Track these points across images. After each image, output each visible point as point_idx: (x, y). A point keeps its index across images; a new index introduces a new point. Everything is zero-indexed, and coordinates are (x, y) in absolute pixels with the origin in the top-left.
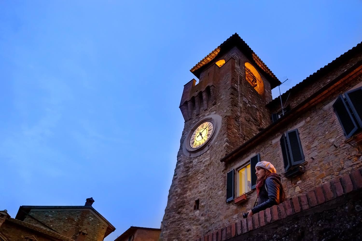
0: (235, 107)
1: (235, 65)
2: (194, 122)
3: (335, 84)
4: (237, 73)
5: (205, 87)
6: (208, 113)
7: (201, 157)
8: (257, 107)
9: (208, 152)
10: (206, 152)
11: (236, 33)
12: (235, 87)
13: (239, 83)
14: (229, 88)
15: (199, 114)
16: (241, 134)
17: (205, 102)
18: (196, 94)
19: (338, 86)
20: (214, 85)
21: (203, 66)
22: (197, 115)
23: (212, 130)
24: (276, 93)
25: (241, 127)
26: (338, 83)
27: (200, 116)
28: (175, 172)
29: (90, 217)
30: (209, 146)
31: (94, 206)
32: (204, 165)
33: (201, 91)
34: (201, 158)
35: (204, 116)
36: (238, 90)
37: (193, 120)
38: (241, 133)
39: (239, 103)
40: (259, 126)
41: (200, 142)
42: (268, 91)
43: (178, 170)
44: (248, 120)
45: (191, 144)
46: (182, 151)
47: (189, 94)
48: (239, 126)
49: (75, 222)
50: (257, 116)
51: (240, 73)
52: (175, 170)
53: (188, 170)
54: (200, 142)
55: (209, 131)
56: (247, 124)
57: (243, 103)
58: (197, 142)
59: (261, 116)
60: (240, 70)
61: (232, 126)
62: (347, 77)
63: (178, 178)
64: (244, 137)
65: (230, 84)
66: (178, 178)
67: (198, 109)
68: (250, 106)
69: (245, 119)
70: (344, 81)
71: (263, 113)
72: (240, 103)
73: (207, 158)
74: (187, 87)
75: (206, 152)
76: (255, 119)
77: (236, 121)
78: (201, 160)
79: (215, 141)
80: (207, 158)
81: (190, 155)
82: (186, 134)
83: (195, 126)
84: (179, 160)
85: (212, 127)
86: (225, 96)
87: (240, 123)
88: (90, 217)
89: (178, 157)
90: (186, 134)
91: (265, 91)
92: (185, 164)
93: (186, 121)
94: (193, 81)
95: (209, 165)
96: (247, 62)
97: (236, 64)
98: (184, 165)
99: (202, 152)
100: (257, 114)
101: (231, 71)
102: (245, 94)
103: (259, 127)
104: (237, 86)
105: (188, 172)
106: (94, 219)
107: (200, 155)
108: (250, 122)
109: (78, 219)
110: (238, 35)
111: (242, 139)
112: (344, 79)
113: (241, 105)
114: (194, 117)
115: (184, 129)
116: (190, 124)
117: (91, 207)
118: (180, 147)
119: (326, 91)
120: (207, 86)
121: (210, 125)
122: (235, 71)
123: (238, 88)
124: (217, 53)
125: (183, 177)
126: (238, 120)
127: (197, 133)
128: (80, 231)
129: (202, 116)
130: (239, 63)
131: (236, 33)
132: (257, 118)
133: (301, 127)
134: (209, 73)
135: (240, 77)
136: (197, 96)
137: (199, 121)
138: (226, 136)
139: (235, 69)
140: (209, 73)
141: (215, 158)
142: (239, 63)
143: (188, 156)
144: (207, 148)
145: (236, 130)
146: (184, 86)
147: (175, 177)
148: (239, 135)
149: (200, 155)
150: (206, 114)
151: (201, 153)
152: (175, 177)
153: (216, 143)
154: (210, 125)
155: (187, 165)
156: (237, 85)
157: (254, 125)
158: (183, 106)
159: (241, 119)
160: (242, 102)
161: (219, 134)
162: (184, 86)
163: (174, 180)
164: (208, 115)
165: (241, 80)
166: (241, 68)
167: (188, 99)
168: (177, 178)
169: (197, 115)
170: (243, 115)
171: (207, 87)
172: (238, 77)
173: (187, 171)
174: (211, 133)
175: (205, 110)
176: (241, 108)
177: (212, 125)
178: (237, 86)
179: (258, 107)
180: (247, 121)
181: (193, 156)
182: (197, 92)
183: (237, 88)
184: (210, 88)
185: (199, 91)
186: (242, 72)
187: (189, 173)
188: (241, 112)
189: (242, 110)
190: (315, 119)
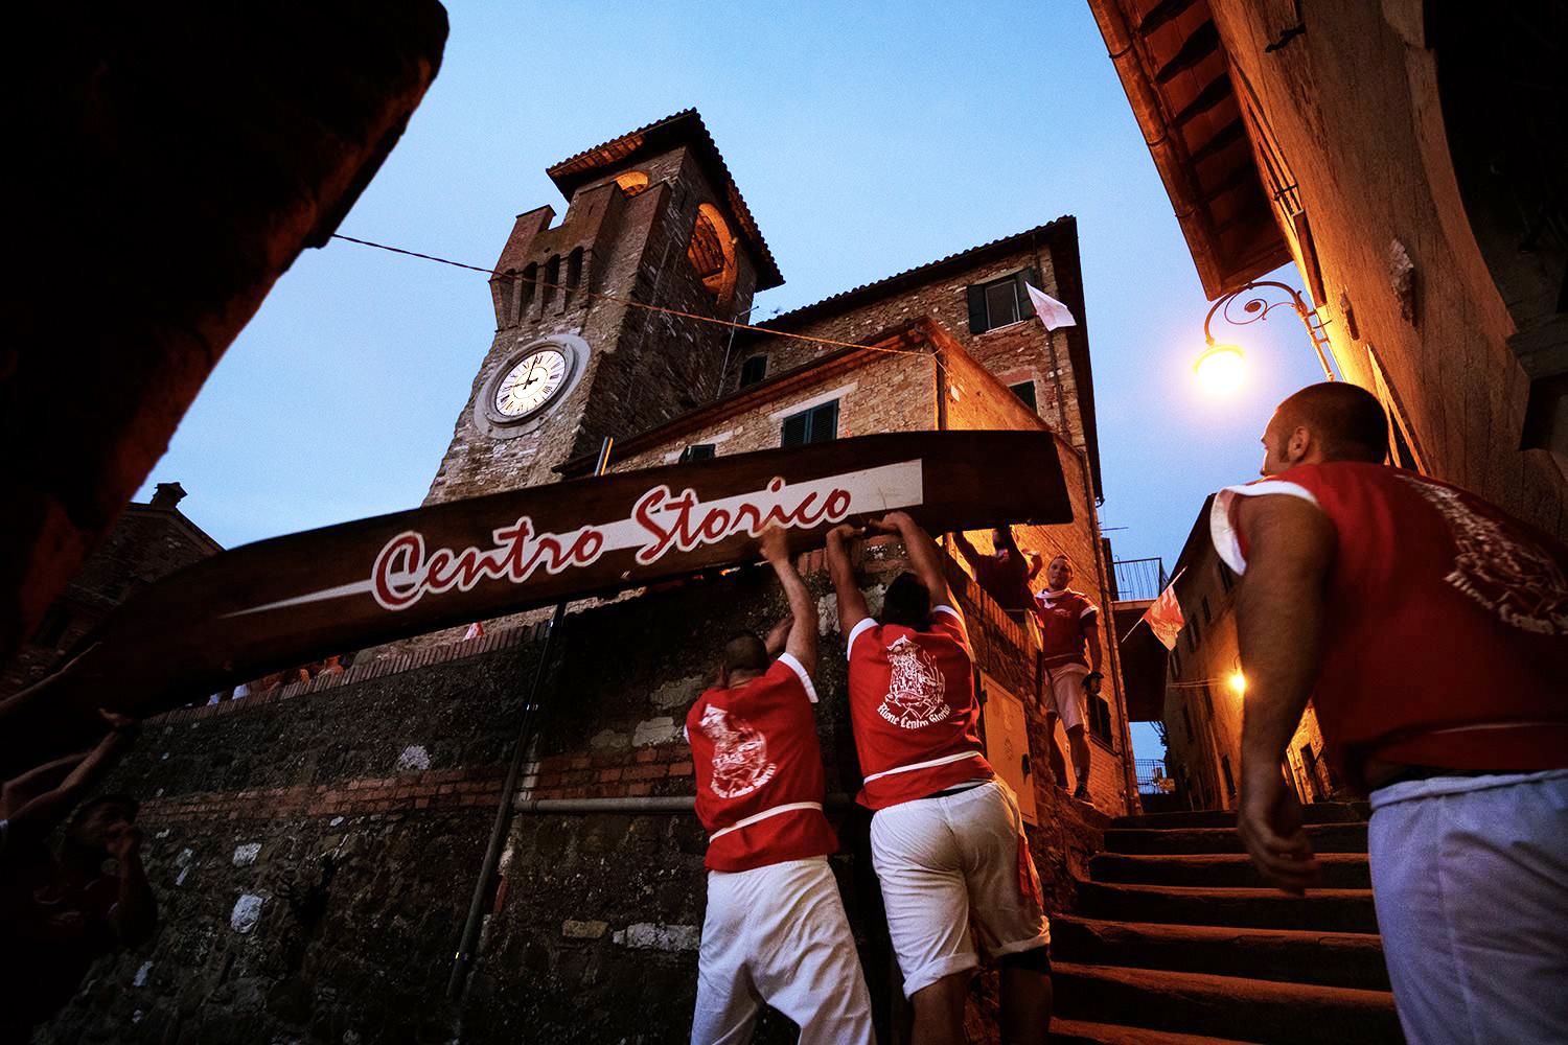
0: (633, 333)
1: (667, 205)
2: (521, 339)
3: (803, 375)
4: (668, 233)
5: (572, 249)
6: (562, 327)
7: (515, 443)
8: (695, 338)
9: (537, 434)
10: (531, 433)
11: (694, 109)
12: (650, 275)
13: (662, 266)
14: (630, 273)
15: (540, 321)
16: (627, 409)
17: (561, 293)
18: (542, 258)
19: (806, 378)
20: (596, 250)
21: (586, 170)
22: (533, 322)
23: (560, 377)
24: (766, 306)
25: (633, 391)
26: (806, 374)
27: (540, 327)
28: (443, 465)
29: (170, 539)
30: (542, 419)
31: (183, 506)
32: (519, 465)
33: (535, 263)
34: (516, 446)
35: (550, 331)
36: (653, 283)
37: (520, 332)
38: (626, 405)
39: (646, 324)
40: (682, 391)
41: (522, 401)
42: (744, 298)
43: (452, 462)
44: (656, 372)
45: (498, 401)
46: (472, 413)
47: (525, 249)
48: (626, 387)
49: (115, 546)
50: (689, 362)
51: (676, 234)
52: (443, 460)
53: (474, 469)
54: (522, 401)
55: (553, 380)
56: (653, 382)
57: (656, 323)
58: (514, 399)
59: (699, 363)
60: (678, 223)
61: (607, 387)
62: (826, 366)
63: (448, 483)
64: (633, 417)
65: (636, 263)
66: (448, 483)
67: (541, 305)
68: (675, 334)
69: (650, 368)
70: (819, 373)
71: (707, 356)
72: (649, 322)
73: (530, 451)
74: (524, 223)
75: (531, 433)
76: (678, 373)
77: (624, 371)
78: (513, 452)
79: (559, 413)
80: (530, 451)
81: (490, 431)
82: (492, 368)
83: (518, 354)
84: (458, 436)
85: (562, 372)
86: (617, 289)
87: (632, 378)
88: (170, 539)
89: (458, 425)
90: (492, 368)
91: (734, 297)
92: (472, 450)
93: (500, 330)
94: (548, 212)
95: (529, 467)
96: (707, 203)
97: (671, 205)
98: (468, 454)
99: (522, 430)
100: (690, 359)
101: (649, 224)
102: (672, 297)
103: (682, 395)
104: (654, 271)
105: (477, 474)
106: (185, 545)
107: (515, 439)
108: (662, 379)
109: (124, 538)
110: (699, 116)
111: (625, 421)
112: (819, 369)
113: (651, 329)
114: (525, 325)
115: (491, 352)
116: (510, 343)
117: (172, 510)
118: (470, 400)
119: (786, 383)
120: (576, 245)
121: (558, 364)
122: (661, 226)
123: (655, 277)
124: (632, 147)
125: (459, 484)
126: (631, 368)
127: (520, 373)
128: (133, 575)
129: (544, 329)
130: (682, 204)
131: (694, 109)
132: (686, 368)
133: (722, 443)
134: (592, 208)
135: (671, 246)
136: (545, 265)
137: (534, 343)
138: (583, 407)
139: (664, 219)
140: (592, 208)
141: (546, 456)
142: (682, 204)
143: (485, 432)
144: (535, 424)
145: (614, 396)
146: (517, 217)
147: (440, 479)
148: (620, 409)
149: (515, 439)
150: (557, 329)
151: (518, 432)
152: (440, 479)
153: (559, 417)
154: (558, 364)
155: (478, 456)
156: (657, 270)
157: (670, 387)
158: (502, 280)
159: (638, 368)
160: (656, 321)
161: (572, 395)
162: (517, 217)
163: (437, 485)
164: (562, 331)
165: (671, 257)
166: (683, 221)
167: (519, 265)
168: (444, 483)
169: (533, 322)
170: (649, 357)
171: (577, 248)
172: (665, 245)
173: (474, 471)
174: (554, 387)
175: (557, 313)
176: (647, 335)
177: (563, 364)
178: (654, 271)
179: (698, 340)
180: (652, 374)
181: (497, 433)
182: (546, 251)
183: (653, 279)
184: (581, 256)
185: (551, 253)
186: (682, 233)
187: (477, 478)
188: (645, 348)
189: (650, 343)
190: (750, 435)
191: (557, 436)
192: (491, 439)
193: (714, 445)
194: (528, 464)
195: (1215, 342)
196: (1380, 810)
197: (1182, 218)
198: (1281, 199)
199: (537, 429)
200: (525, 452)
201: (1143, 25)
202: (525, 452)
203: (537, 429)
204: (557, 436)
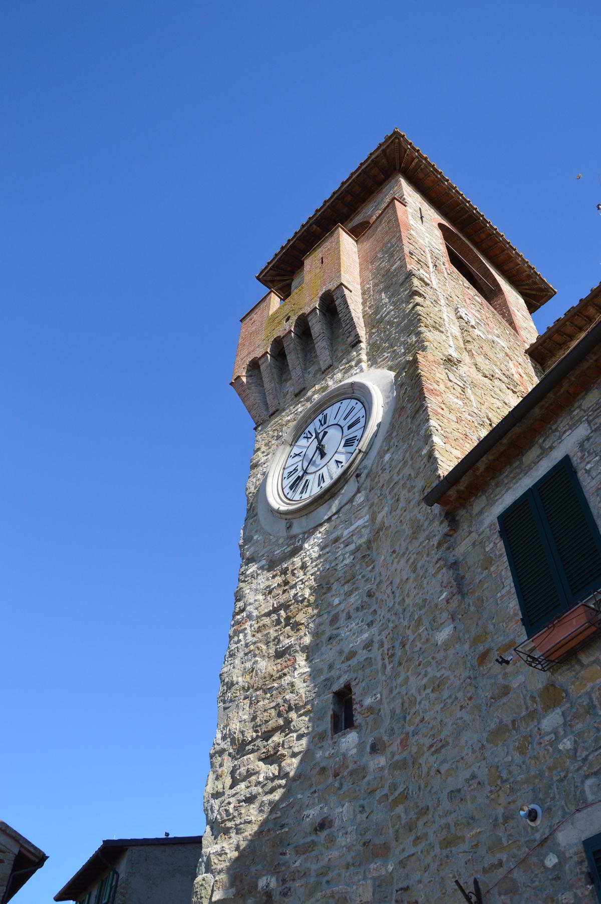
10: (351, 500)
32: (352, 547)
58: (342, 423)
75: (351, 500)
95: (369, 542)
143: (283, 533)
153: (387, 457)
191: (396, 479)
192: (295, 536)
193: (567, 459)
194: (364, 540)
195: (423, 505)
196: (130, 848)
197: (15, 832)
198: (593, 629)
199: (358, 491)
200: (352, 528)
201: (293, 777)
202: (352, 528)
203: (358, 491)
204: (396, 479)
